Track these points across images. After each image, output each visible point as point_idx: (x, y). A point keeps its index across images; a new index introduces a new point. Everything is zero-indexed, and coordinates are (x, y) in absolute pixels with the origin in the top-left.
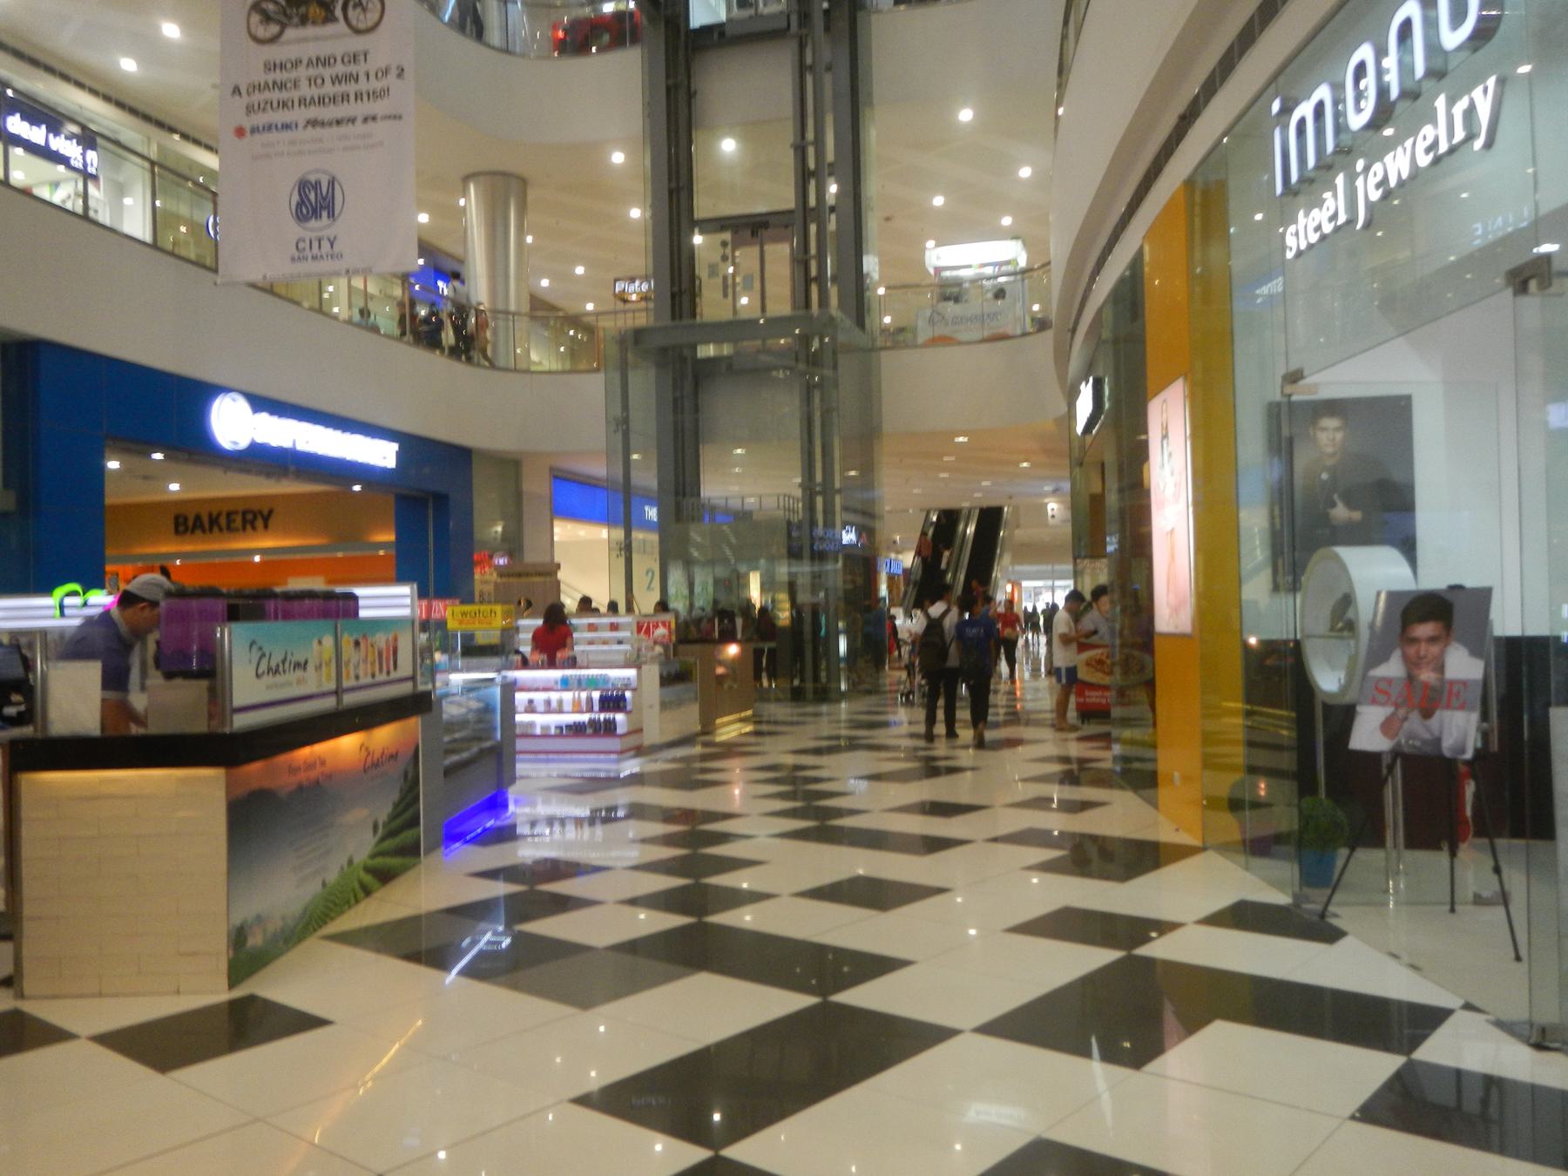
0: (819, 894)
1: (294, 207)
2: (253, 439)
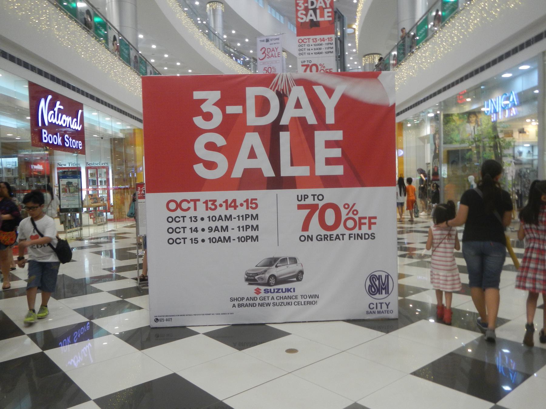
0: (124, 227)
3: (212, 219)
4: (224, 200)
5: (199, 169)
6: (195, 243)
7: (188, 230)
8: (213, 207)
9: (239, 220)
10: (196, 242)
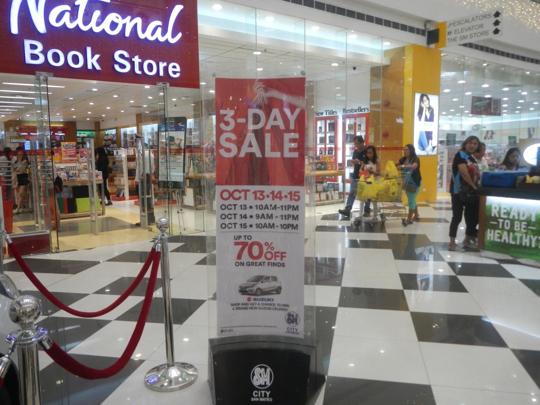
1: (287, 320)
3: (260, 207)
4: (271, 191)
5: (117, 67)
6: (244, 227)
7: (238, 217)
8: (261, 197)
9: (282, 209)
10: (245, 227)
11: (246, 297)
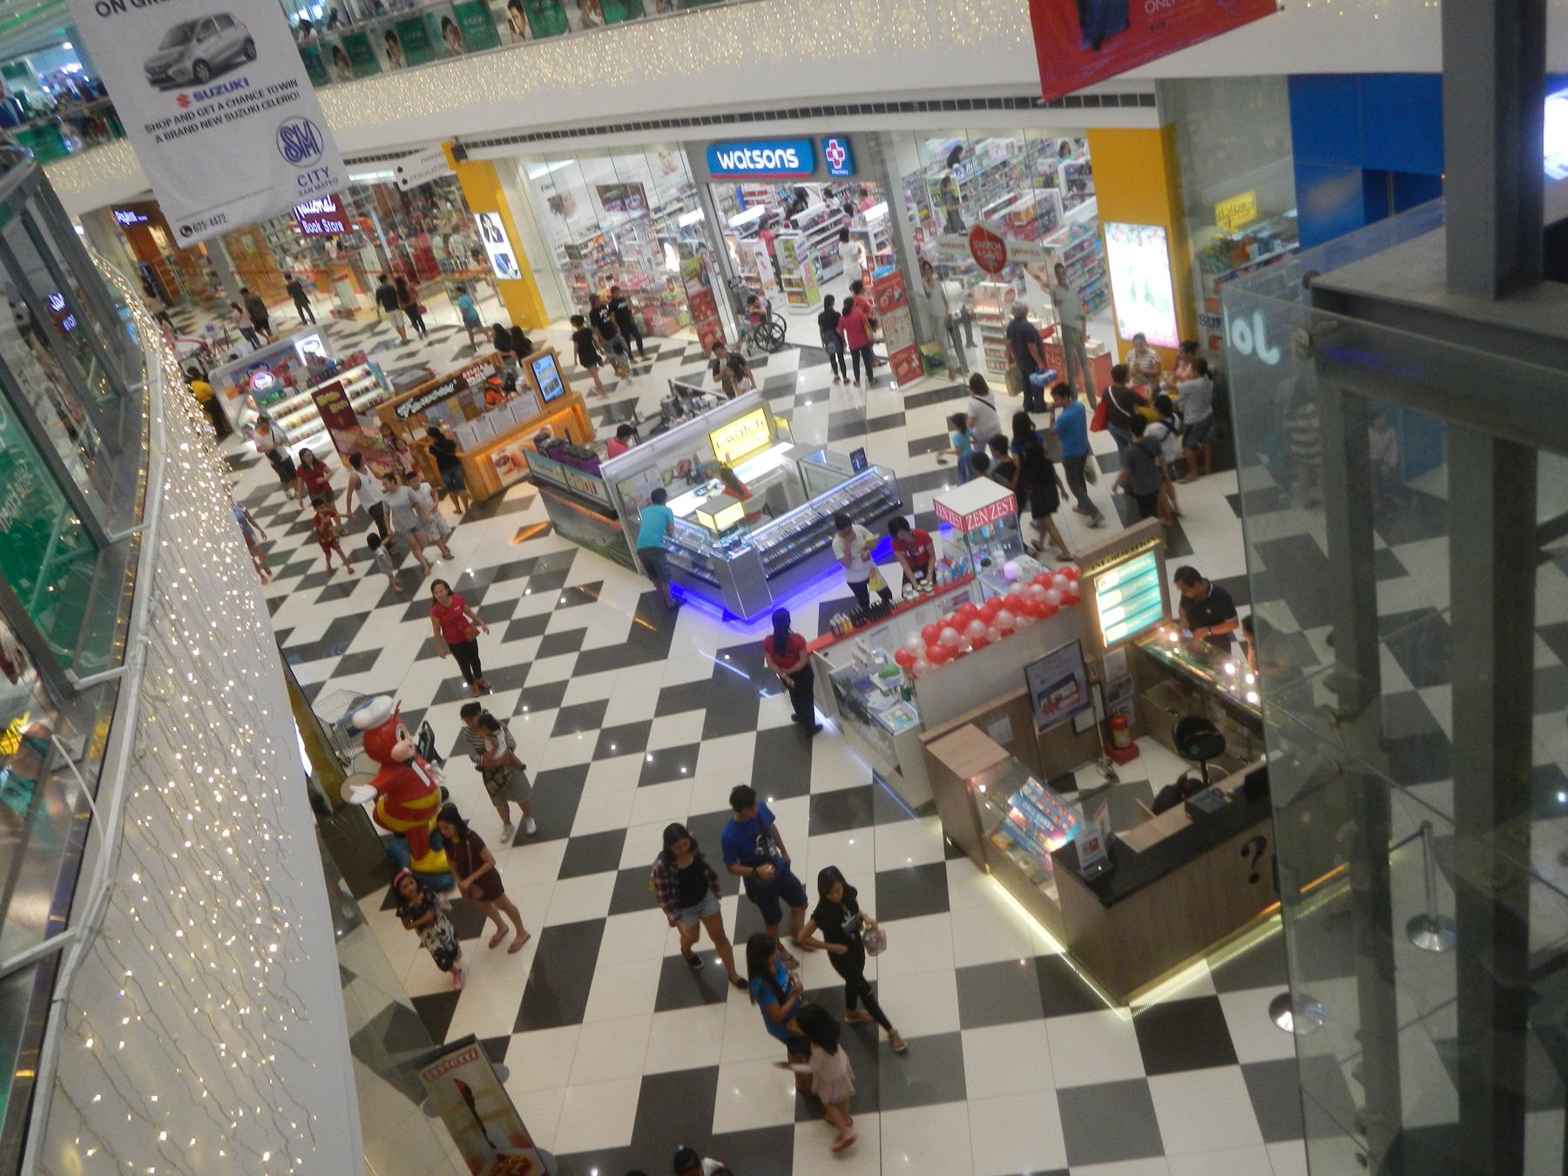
2: (813, 831)
11: (173, 94)
